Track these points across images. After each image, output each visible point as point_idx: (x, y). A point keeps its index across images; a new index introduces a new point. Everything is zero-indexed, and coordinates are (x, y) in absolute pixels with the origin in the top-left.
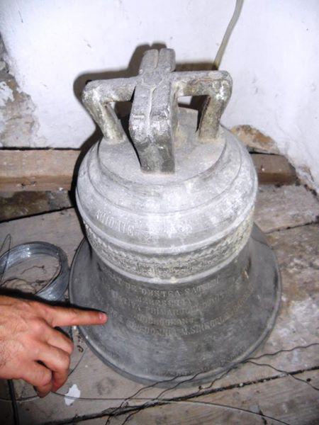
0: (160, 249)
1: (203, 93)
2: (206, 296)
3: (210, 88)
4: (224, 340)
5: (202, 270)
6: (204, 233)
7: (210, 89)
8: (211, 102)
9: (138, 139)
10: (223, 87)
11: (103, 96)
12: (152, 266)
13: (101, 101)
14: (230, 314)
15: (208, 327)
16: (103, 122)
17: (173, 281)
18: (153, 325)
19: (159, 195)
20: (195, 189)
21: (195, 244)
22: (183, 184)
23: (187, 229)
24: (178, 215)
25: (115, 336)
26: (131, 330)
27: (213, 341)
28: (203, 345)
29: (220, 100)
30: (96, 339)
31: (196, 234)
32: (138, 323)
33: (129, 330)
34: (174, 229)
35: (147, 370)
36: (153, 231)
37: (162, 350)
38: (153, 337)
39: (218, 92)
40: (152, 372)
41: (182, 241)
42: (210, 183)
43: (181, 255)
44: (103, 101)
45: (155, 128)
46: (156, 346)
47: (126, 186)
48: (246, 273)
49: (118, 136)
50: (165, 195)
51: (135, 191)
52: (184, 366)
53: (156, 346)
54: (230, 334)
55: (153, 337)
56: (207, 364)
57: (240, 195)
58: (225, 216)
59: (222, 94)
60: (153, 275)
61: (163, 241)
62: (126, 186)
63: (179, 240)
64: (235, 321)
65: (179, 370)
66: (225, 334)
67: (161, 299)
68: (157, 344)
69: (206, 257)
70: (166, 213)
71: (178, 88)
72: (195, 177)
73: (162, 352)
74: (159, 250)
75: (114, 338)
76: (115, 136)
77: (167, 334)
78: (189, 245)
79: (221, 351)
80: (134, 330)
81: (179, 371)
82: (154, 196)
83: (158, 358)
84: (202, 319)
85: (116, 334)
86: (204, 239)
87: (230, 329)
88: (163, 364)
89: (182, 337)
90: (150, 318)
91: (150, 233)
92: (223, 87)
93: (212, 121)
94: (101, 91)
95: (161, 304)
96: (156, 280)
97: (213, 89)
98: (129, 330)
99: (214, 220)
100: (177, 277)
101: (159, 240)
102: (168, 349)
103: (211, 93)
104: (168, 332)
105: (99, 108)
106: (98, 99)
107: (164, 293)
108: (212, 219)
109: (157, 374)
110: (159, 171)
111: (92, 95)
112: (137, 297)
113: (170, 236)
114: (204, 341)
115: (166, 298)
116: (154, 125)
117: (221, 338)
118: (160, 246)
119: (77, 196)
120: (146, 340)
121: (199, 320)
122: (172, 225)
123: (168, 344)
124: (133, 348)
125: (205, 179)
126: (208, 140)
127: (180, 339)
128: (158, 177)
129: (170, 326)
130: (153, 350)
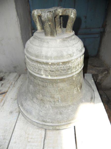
0: (45, 60)
1: (67, 14)
2: (62, 90)
3: (69, 13)
4: (67, 112)
5: (60, 75)
6: (61, 57)
7: (69, 13)
8: (69, 18)
9: (43, 19)
10: (73, 13)
11: (37, 13)
12: (43, 69)
13: (37, 15)
14: (71, 102)
15: (61, 105)
16: (37, 23)
17: (49, 77)
18: (42, 100)
19: (48, 42)
20: (60, 42)
21: (57, 61)
22: (56, 40)
23: (55, 54)
24: (53, 49)
25: (28, 104)
26: (34, 102)
27: (63, 111)
28: (59, 112)
29: (72, 17)
30: (22, 106)
31: (58, 56)
32: (37, 99)
33: (34, 102)
34: (51, 53)
35: (36, 118)
36: (44, 53)
37: (43, 111)
38: (41, 105)
39: (72, 14)
40: (38, 119)
41: (53, 58)
42: (66, 42)
43: (53, 64)
44: (37, 15)
45: (48, 15)
46: (42, 109)
47: (39, 39)
48: (79, 88)
49: (41, 29)
50: (50, 42)
51: (41, 41)
52: (50, 119)
53: (42, 109)
54: (70, 110)
55: (41, 105)
56: (59, 120)
57: (75, 49)
58: (69, 53)
59: (73, 15)
60: (43, 74)
61: (47, 57)
62: (39, 39)
63: (51, 57)
64: (72, 106)
65: (48, 120)
66: (68, 110)
67: (45, 87)
68: (42, 108)
69: (61, 69)
70: (49, 48)
71: (60, 12)
72: (60, 38)
73: (43, 112)
74: (45, 61)
75: (28, 105)
76: (40, 28)
77: (46, 105)
78: (55, 61)
79: (65, 116)
80: (35, 102)
81: (48, 120)
82: (46, 42)
83: (41, 114)
84: (60, 101)
85: (29, 104)
86: (61, 59)
87: (70, 109)
88: (43, 117)
89: (52, 107)
90: (41, 96)
91: (43, 53)
92: (73, 13)
93: (69, 25)
94: (37, 11)
95: (45, 89)
96: (44, 76)
97: (70, 13)
98: (34, 102)
99: (65, 54)
100: (51, 76)
101: (45, 56)
102: (46, 111)
103: (69, 14)
104: (47, 104)
105: (36, 17)
106: (36, 14)
107: (46, 84)
108: (64, 53)
109: (40, 120)
110: (50, 36)
111: (34, 12)
112: (37, 86)
113: (49, 55)
114: (59, 110)
115: (47, 87)
116: (48, 14)
117: (66, 111)
118: (45, 59)
119: (20, 26)
120: (39, 106)
121: (58, 101)
122: (50, 52)
123: (46, 109)
124: (34, 109)
125: (64, 40)
126: (68, 33)
127: (50, 107)
128: (49, 37)
129: (47, 101)
130: (40, 110)
